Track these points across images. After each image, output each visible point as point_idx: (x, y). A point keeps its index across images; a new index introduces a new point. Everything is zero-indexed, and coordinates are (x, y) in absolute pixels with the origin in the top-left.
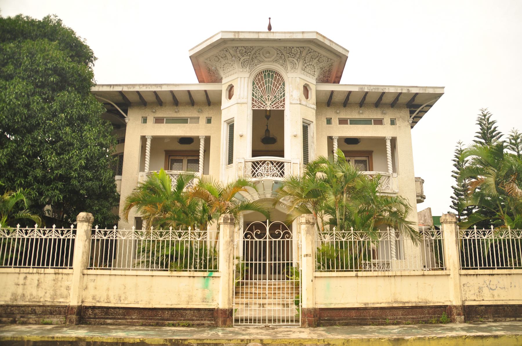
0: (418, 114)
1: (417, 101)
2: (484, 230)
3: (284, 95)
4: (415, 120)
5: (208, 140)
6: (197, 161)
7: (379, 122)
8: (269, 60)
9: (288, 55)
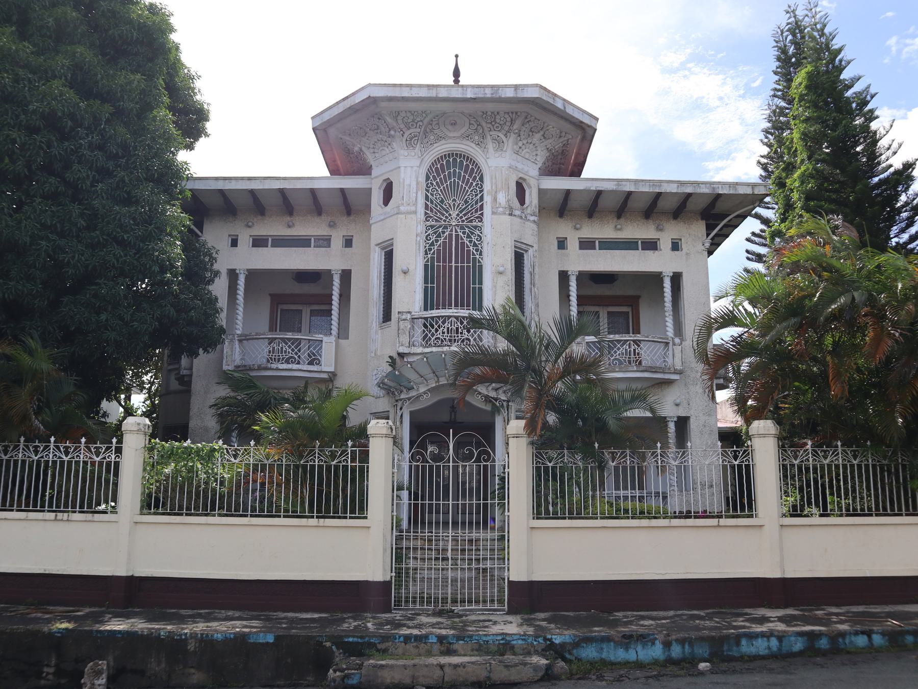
0: (721, 230)
1: (720, 207)
2: (824, 448)
3: (482, 198)
4: (717, 240)
5: (346, 276)
6: (329, 313)
7: (651, 245)
8: (456, 134)
9: (489, 126)
